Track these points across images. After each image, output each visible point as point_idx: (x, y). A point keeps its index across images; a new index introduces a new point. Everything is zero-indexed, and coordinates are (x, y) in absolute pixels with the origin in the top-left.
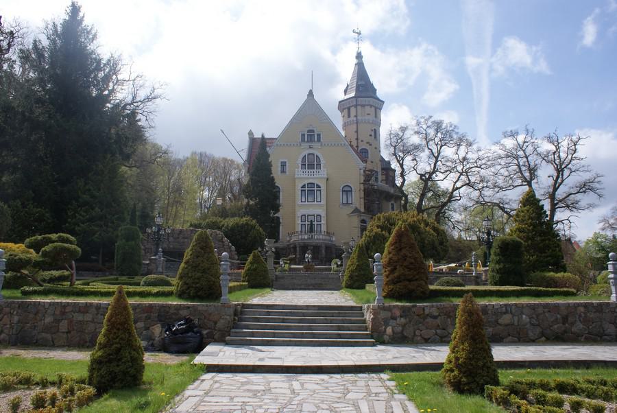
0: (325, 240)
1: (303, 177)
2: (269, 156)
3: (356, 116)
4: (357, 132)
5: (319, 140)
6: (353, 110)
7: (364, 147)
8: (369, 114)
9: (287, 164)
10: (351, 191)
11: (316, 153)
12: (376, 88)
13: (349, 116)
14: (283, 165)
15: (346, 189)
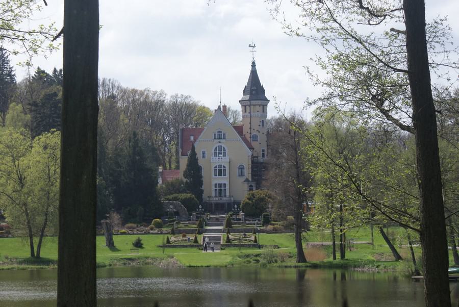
0: (226, 200)
1: (216, 161)
2: (196, 154)
3: (250, 113)
4: (250, 123)
5: (224, 138)
6: (248, 107)
7: (255, 134)
8: (258, 111)
9: (206, 153)
10: (244, 168)
11: (223, 145)
12: (196, 152)
13: (246, 112)
14: (204, 153)
15: (241, 167)
